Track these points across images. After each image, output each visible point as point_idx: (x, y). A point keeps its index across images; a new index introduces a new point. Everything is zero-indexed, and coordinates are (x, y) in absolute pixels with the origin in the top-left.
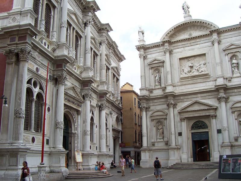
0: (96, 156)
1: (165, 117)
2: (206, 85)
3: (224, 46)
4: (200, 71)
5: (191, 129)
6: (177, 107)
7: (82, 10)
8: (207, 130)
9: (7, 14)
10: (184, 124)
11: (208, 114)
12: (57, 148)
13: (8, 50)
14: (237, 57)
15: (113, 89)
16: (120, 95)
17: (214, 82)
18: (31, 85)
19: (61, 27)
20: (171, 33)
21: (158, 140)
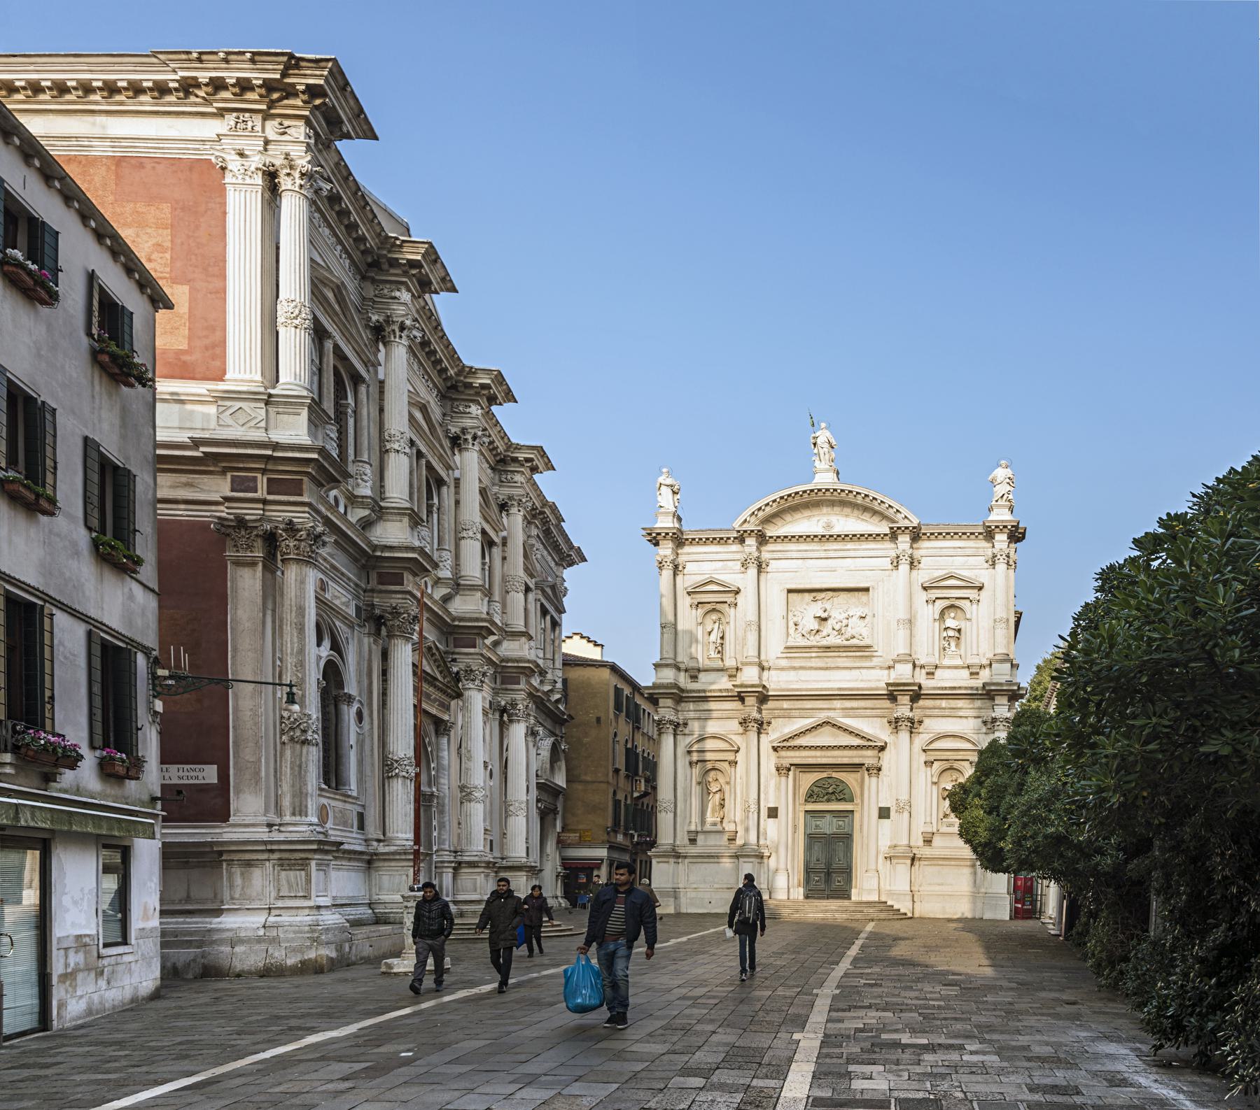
0: (358, 860)
1: (730, 757)
4: (848, 635)
7: (439, 391)
8: (848, 807)
11: (857, 761)
12: (398, 842)
16: (560, 674)
17: (886, 672)
20: (768, 509)
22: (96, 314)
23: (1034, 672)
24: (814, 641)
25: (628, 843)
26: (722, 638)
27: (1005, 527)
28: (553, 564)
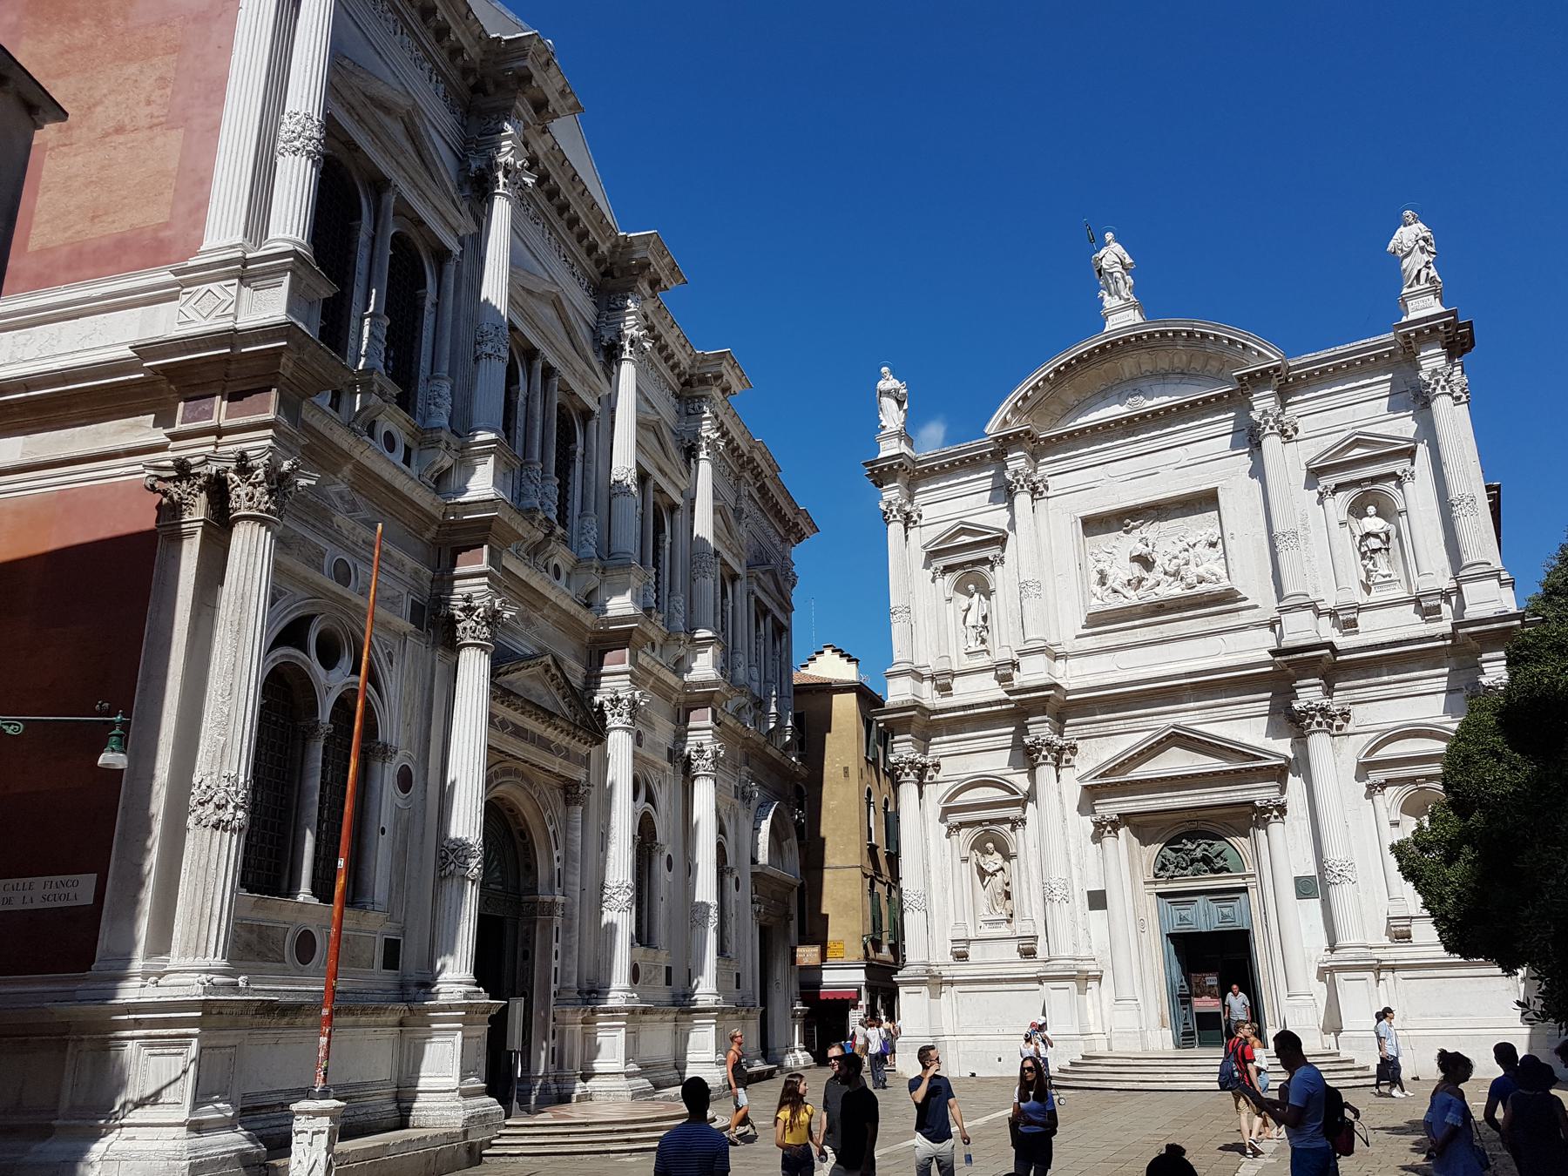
1: (1013, 813)
3: (1307, 451)
6: (1076, 760)
8: (1238, 883)
9: (172, 277)
13: (170, 463)
15: (756, 677)
18: (305, 650)
19: (477, 359)
21: (988, 932)
22: (428, 305)
24: (1133, 598)
26: (985, 618)
27: (1434, 329)
28: (777, 540)
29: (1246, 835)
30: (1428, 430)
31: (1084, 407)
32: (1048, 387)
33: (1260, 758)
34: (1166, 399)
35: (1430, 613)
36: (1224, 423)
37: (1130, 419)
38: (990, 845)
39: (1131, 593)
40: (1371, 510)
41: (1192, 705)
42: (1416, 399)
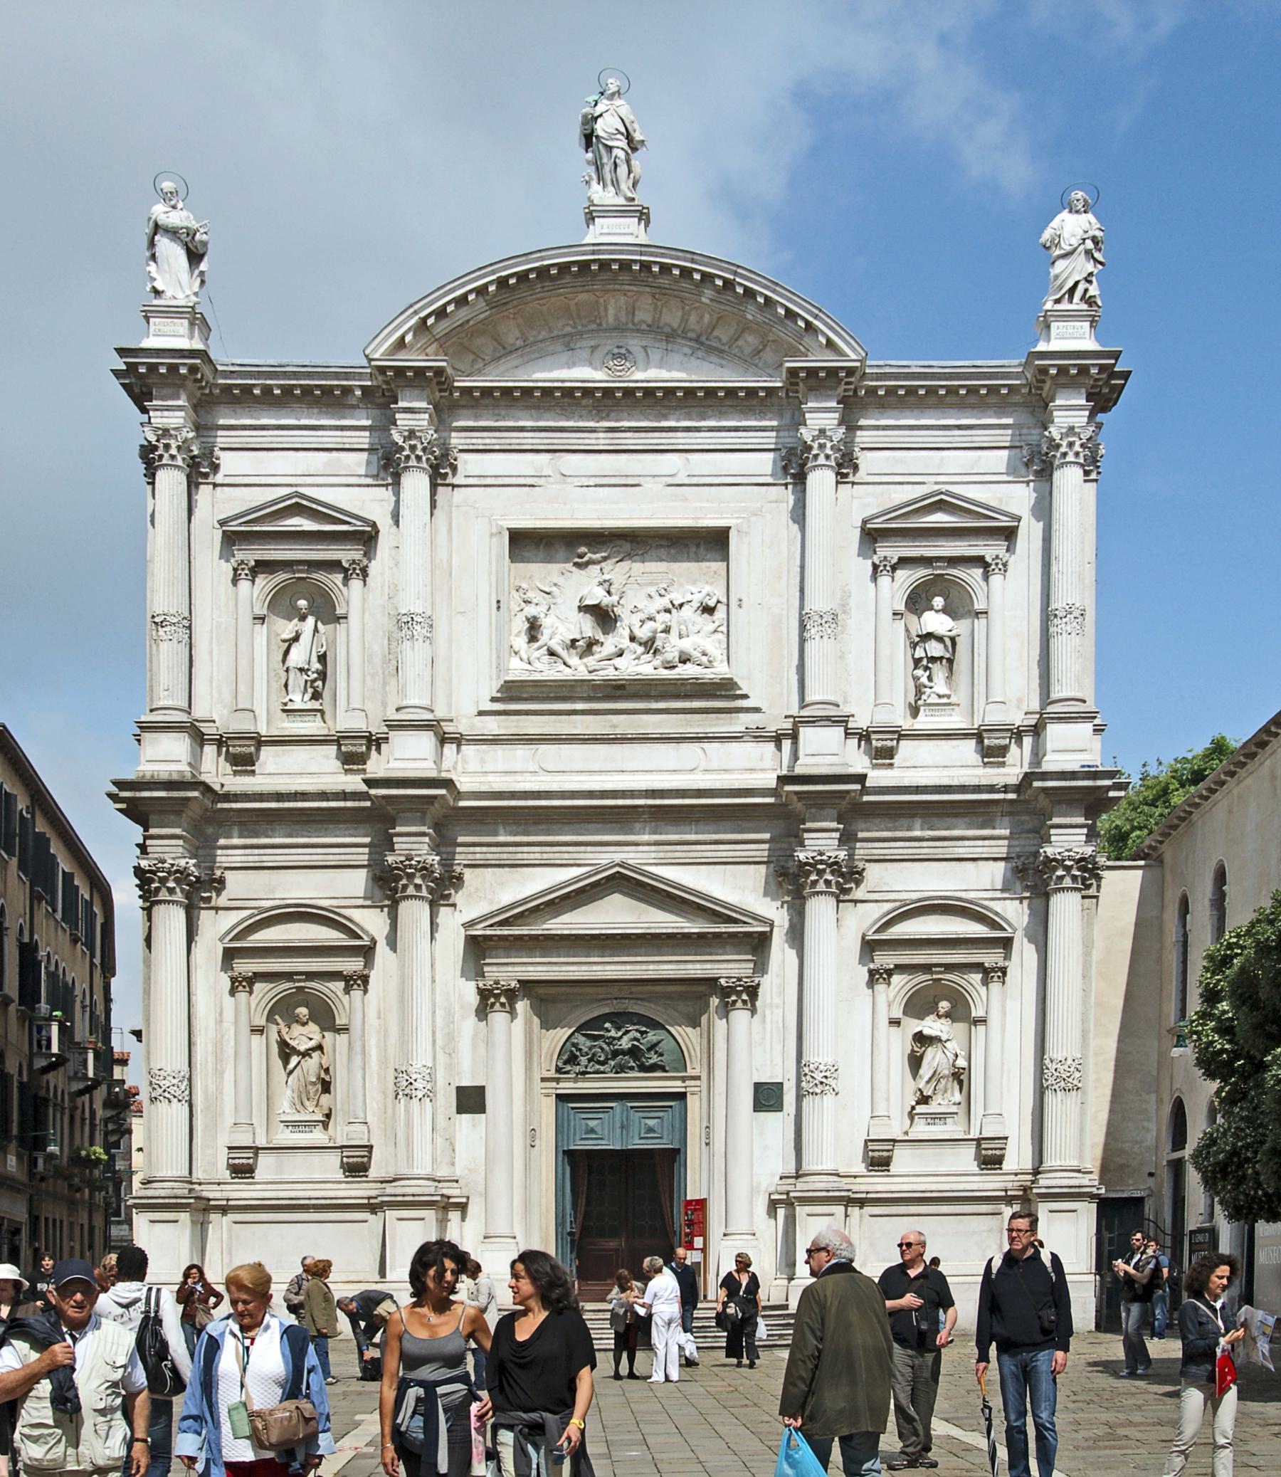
1: (352, 965)
2: (703, 765)
3: (866, 502)
4: (672, 654)
5: (558, 1070)
6: (459, 897)
8: (675, 1086)
10: (514, 1028)
14: (954, 592)
21: (287, 1137)
23: (1201, 745)
24: (578, 668)
25: (23, 1177)
27: (1083, 370)
29: (695, 1023)
30: (1044, 509)
31: (529, 350)
32: (482, 304)
33: (736, 921)
34: (665, 374)
35: (993, 754)
36: (763, 431)
37: (608, 392)
38: (303, 1011)
39: (574, 660)
40: (938, 602)
41: (646, 838)
42: (1039, 464)
